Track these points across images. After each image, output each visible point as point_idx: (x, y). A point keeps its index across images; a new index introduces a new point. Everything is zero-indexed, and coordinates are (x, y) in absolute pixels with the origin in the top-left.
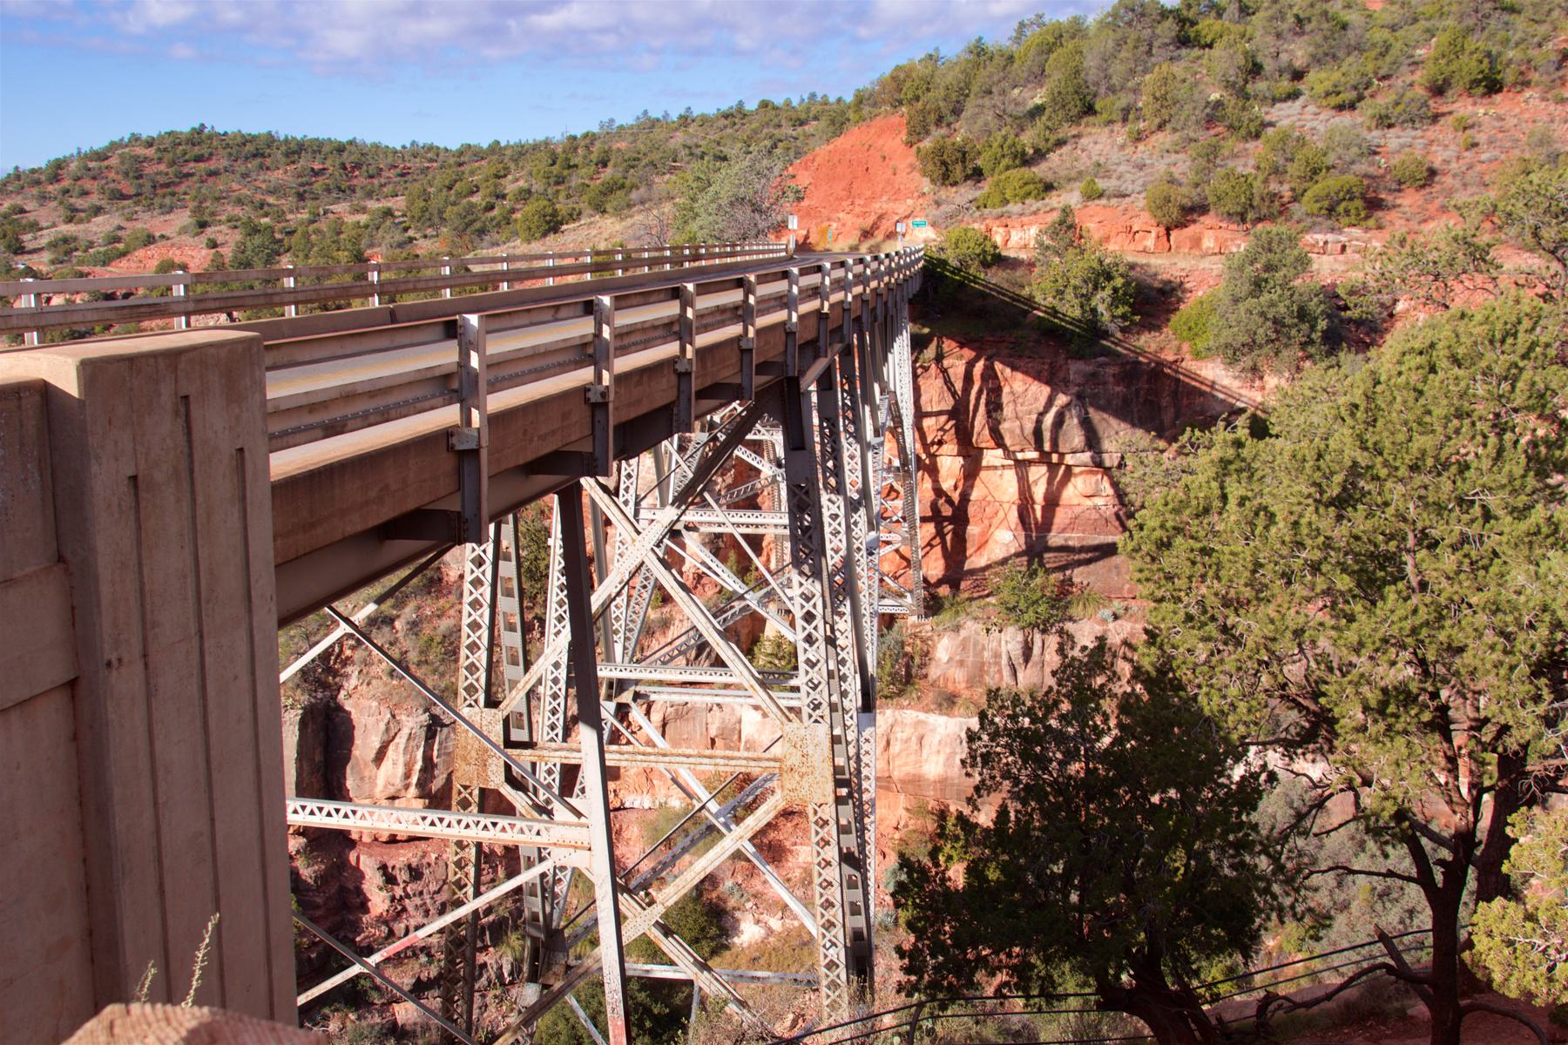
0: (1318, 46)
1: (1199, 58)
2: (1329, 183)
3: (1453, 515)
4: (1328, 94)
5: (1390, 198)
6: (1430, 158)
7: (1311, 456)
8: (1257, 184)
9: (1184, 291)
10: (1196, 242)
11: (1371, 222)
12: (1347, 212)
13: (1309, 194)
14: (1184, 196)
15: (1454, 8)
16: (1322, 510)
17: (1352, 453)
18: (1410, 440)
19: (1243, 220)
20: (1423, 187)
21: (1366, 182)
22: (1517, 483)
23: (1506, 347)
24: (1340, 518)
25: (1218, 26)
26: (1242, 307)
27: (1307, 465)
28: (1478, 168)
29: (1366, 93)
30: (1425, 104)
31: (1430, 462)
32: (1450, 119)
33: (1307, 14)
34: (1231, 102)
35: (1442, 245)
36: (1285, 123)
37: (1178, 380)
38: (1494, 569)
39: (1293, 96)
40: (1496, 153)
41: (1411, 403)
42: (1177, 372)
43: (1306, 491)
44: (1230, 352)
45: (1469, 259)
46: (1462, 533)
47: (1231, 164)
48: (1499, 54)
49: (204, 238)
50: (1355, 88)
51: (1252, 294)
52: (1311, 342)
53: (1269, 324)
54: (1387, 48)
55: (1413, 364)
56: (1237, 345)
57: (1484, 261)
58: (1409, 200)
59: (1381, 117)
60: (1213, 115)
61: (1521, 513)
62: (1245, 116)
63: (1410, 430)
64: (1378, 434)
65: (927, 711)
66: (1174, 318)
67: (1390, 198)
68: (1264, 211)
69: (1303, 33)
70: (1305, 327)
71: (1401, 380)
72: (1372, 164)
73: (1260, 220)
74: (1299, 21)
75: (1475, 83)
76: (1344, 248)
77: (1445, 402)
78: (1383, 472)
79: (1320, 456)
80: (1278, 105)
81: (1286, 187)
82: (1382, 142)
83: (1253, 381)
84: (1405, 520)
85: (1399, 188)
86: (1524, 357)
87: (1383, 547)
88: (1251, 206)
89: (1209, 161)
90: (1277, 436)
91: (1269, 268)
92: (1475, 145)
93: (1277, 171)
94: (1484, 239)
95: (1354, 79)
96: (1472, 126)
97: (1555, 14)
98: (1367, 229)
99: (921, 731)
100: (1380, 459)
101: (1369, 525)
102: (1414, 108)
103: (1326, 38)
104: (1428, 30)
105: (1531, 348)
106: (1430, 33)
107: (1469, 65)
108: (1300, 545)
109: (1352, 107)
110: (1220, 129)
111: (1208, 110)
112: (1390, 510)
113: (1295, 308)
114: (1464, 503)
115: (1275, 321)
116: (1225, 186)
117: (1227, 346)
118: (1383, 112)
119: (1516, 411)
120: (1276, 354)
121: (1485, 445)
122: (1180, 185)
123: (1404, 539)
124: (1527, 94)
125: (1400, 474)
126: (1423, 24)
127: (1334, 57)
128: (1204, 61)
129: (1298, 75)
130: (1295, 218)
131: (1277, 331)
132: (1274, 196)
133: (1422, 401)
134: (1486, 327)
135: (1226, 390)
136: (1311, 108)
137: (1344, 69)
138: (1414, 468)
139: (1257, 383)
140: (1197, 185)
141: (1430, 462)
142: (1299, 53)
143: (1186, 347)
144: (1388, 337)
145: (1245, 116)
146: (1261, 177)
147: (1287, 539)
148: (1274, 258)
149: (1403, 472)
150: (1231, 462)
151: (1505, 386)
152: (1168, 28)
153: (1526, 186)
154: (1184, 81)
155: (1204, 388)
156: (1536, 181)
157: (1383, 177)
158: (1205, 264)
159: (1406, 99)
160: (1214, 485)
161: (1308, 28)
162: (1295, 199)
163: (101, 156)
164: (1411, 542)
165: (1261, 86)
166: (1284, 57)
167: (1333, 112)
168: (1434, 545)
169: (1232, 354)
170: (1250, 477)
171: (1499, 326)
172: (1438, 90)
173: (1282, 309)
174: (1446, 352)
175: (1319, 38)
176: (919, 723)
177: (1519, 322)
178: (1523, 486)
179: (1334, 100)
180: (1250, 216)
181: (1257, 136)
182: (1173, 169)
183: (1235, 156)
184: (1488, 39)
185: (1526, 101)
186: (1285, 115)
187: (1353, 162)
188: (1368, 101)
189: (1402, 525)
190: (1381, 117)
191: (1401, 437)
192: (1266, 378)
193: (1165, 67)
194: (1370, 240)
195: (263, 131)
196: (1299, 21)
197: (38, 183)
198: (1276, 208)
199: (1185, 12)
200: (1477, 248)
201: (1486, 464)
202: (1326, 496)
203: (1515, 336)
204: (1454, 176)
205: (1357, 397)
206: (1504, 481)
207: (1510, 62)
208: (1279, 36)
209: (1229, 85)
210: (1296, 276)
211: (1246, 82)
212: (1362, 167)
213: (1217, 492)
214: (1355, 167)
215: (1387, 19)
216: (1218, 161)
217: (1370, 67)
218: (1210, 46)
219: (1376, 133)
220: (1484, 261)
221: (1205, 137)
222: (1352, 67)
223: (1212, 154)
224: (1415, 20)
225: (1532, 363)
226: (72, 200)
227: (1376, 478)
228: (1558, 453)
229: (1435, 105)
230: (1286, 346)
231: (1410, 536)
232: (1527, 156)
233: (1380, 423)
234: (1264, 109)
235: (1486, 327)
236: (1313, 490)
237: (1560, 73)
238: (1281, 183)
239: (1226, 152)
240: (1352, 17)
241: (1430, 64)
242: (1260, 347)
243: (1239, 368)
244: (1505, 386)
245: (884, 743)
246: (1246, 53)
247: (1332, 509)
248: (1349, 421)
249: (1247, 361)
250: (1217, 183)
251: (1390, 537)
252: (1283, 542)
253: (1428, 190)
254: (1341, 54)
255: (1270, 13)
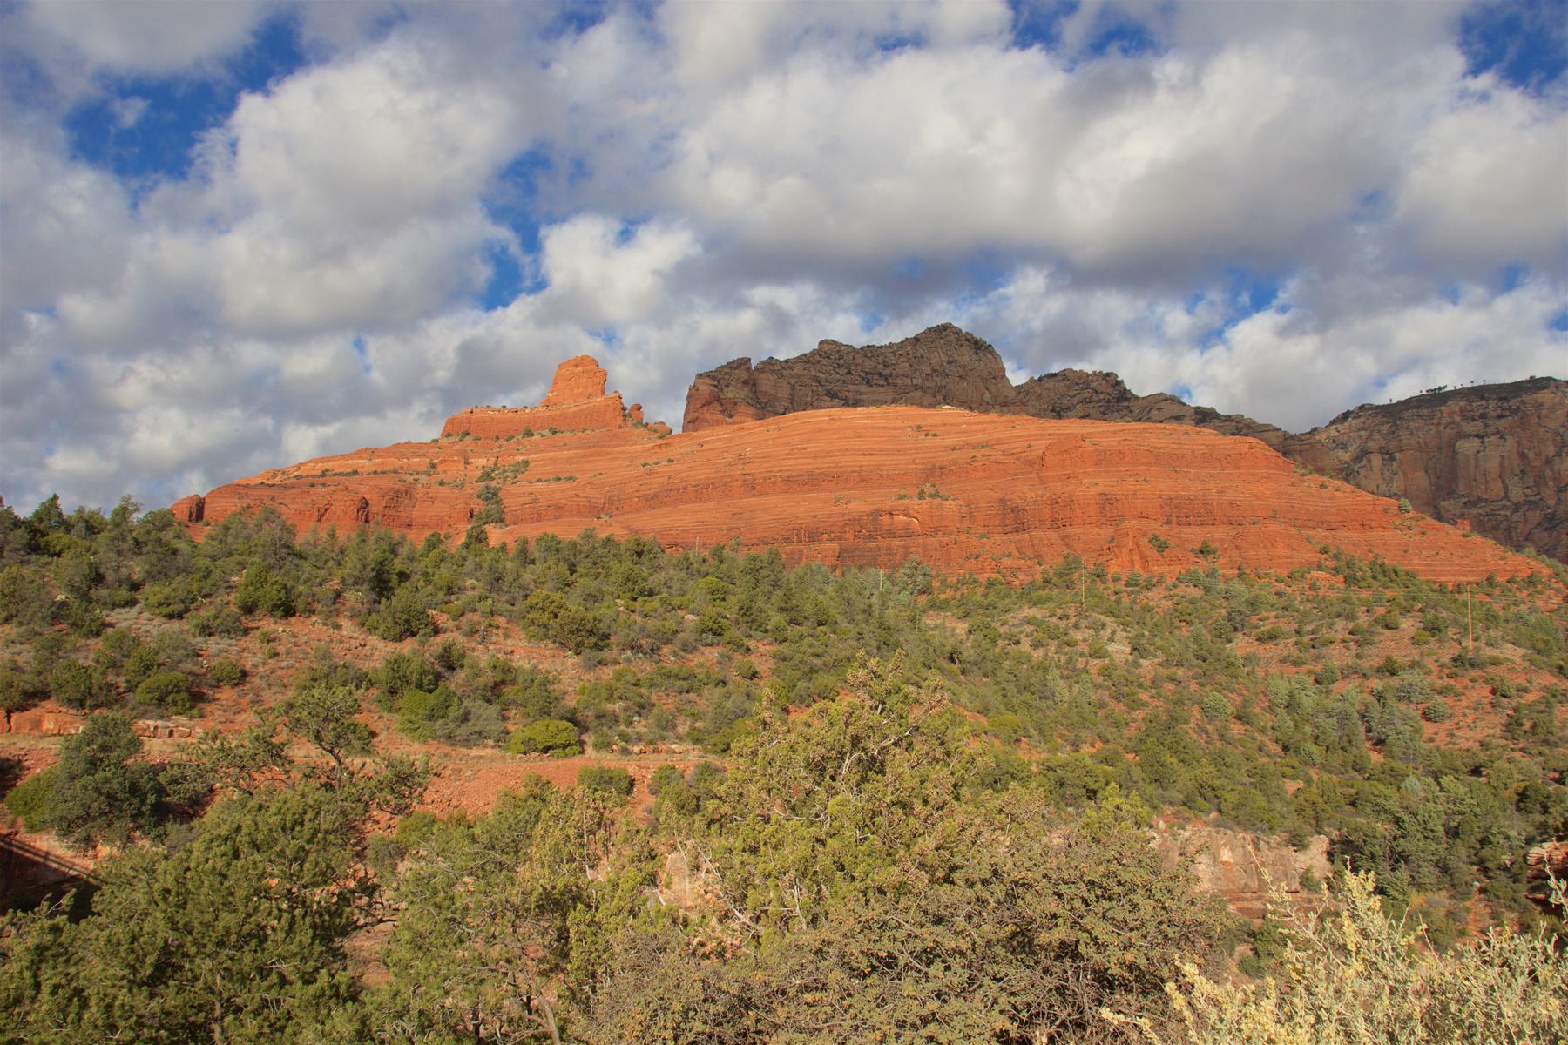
0: (152, 565)
1: (47, 564)
2: (160, 678)
3: (255, 983)
4: (160, 605)
5: (210, 692)
6: (242, 662)
7: (125, 938)
8: (95, 675)
9: (22, 769)
10: (37, 724)
11: (195, 712)
12: (175, 703)
13: (142, 686)
14: (26, 682)
15: (260, 549)
16: (135, 990)
17: (165, 933)
18: (216, 919)
19: (82, 706)
20: (237, 685)
21: (190, 679)
22: (306, 951)
23: (295, 833)
24: (152, 996)
25: (66, 539)
26: (78, 784)
27: (122, 949)
28: (280, 672)
29: (192, 606)
30: (238, 620)
31: (233, 938)
32: (258, 633)
33: (144, 539)
34: (76, 603)
35: (247, 743)
36: (123, 624)
37: (12, 852)
38: (289, 1030)
39: (131, 603)
40: (292, 662)
41: (217, 885)
42: (10, 844)
43: (120, 973)
44: (65, 825)
45: (268, 755)
46: (261, 999)
47: (73, 657)
48: (293, 587)
50: (183, 601)
51: (87, 772)
52: (142, 814)
53: (102, 798)
54: (209, 573)
55: (219, 851)
56: (72, 817)
57: (280, 757)
58: (226, 695)
59: (203, 627)
60: (59, 613)
61: (308, 980)
62: (88, 617)
63: (216, 910)
64: (193, 915)
66: (11, 794)
67: (210, 692)
68: (102, 699)
69: (141, 554)
70: (136, 801)
71: (209, 866)
72: (196, 664)
73: (97, 706)
74: (137, 543)
75: (275, 607)
76: (171, 733)
77: (245, 884)
78: (193, 950)
79: (134, 939)
80: (117, 610)
81: (122, 679)
82: (205, 647)
83: (86, 850)
84: (213, 992)
85: (218, 684)
86: (309, 841)
87: (192, 1019)
88: (90, 694)
89: (52, 653)
90: (100, 915)
91: (105, 748)
92: (276, 654)
93: (115, 665)
94: (283, 736)
95: (182, 594)
96: (274, 640)
97: (330, 563)
98: (192, 718)
100: (190, 938)
101: (179, 999)
102: (229, 622)
103: (159, 560)
104: (240, 563)
105: (314, 835)
106: (242, 565)
107: (271, 593)
108: (113, 1028)
109: (180, 616)
110: (64, 626)
111: (53, 609)
112: (200, 984)
113: (127, 784)
114: (263, 973)
115: (109, 796)
116: (67, 676)
117: (62, 818)
118: (205, 623)
119: (305, 887)
120: (109, 826)
121: (279, 920)
122: (24, 672)
123: (213, 1009)
124: (314, 619)
125: (207, 950)
126: (236, 558)
127: (166, 575)
128: (52, 567)
129: (135, 587)
130: (130, 705)
131: (110, 805)
132: (111, 686)
133: (227, 884)
134: (279, 817)
135: (61, 861)
136: (146, 615)
137: (174, 586)
138: (221, 944)
139: (91, 852)
140: (40, 673)
141: (233, 938)
142: (137, 569)
143: (21, 820)
144: (209, 809)
145: (88, 617)
146: (100, 670)
147: (100, 1023)
148: (109, 740)
149: (210, 948)
150: (47, 948)
151: (295, 866)
152: (20, 536)
153: (310, 699)
154: (33, 582)
155: (37, 858)
156: (317, 695)
157: (205, 674)
158: (44, 744)
159: (223, 615)
160: (27, 974)
161: (145, 550)
162: (130, 690)
164: (218, 1012)
165: (103, 592)
166: (124, 571)
167: (164, 620)
168: (239, 1010)
169: (66, 827)
170: (67, 961)
171: (289, 816)
172: (249, 609)
173: (116, 786)
174: (247, 839)
175: (154, 559)
177: (305, 813)
178: (311, 953)
179: (165, 610)
180: (88, 702)
181: (98, 634)
182: (17, 658)
183: (78, 650)
184: (284, 575)
185: (313, 625)
186: (123, 618)
187: (180, 662)
188: (194, 613)
189: (210, 997)
190: (203, 627)
191: (208, 917)
192: (99, 847)
193: (14, 569)
194: (194, 726)
196: (137, 543)
198: (113, 697)
199: (37, 525)
200: (274, 746)
201: (281, 936)
202: (138, 977)
203: (302, 824)
204: (261, 677)
205: (170, 882)
206: (296, 950)
207: (300, 594)
208: (119, 553)
209: (73, 589)
210: (129, 756)
211: (90, 588)
212: (188, 666)
213: (30, 982)
214: (182, 666)
215: (208, 550)
216: (61, 654)
217: (195, 586)
218: (59, 555)
219: (199, 639)
220: (280, 757)
221: (50, 632)
222: (179, 586)
223: (55, 647)
224: (230, 555)
225: (315, 847)
227: (186, 955)
228: (338, 920)
229: (246, 621)
230: (119, 818)
231: (218, 1006)
232: (315, 666)
233: (189, 906)
234: (105, 612)
235: (279, 817)
236: (126, 972)
237: (337, 606)
238: (118, 675)
239: (69, 646)
240: (182, 546)
241: (242, 588)
242: (94, 819)
243: (72, 839)
244: (295, 866)
246: (90, 564)
247: (144, 988)
248: (162, 906)
249: (81, 832)
250: (59, 672)
251: (200, 1008)
252: (96, 1027)
253: (241, 687)
254: (172, 574)
255: (113, 534)
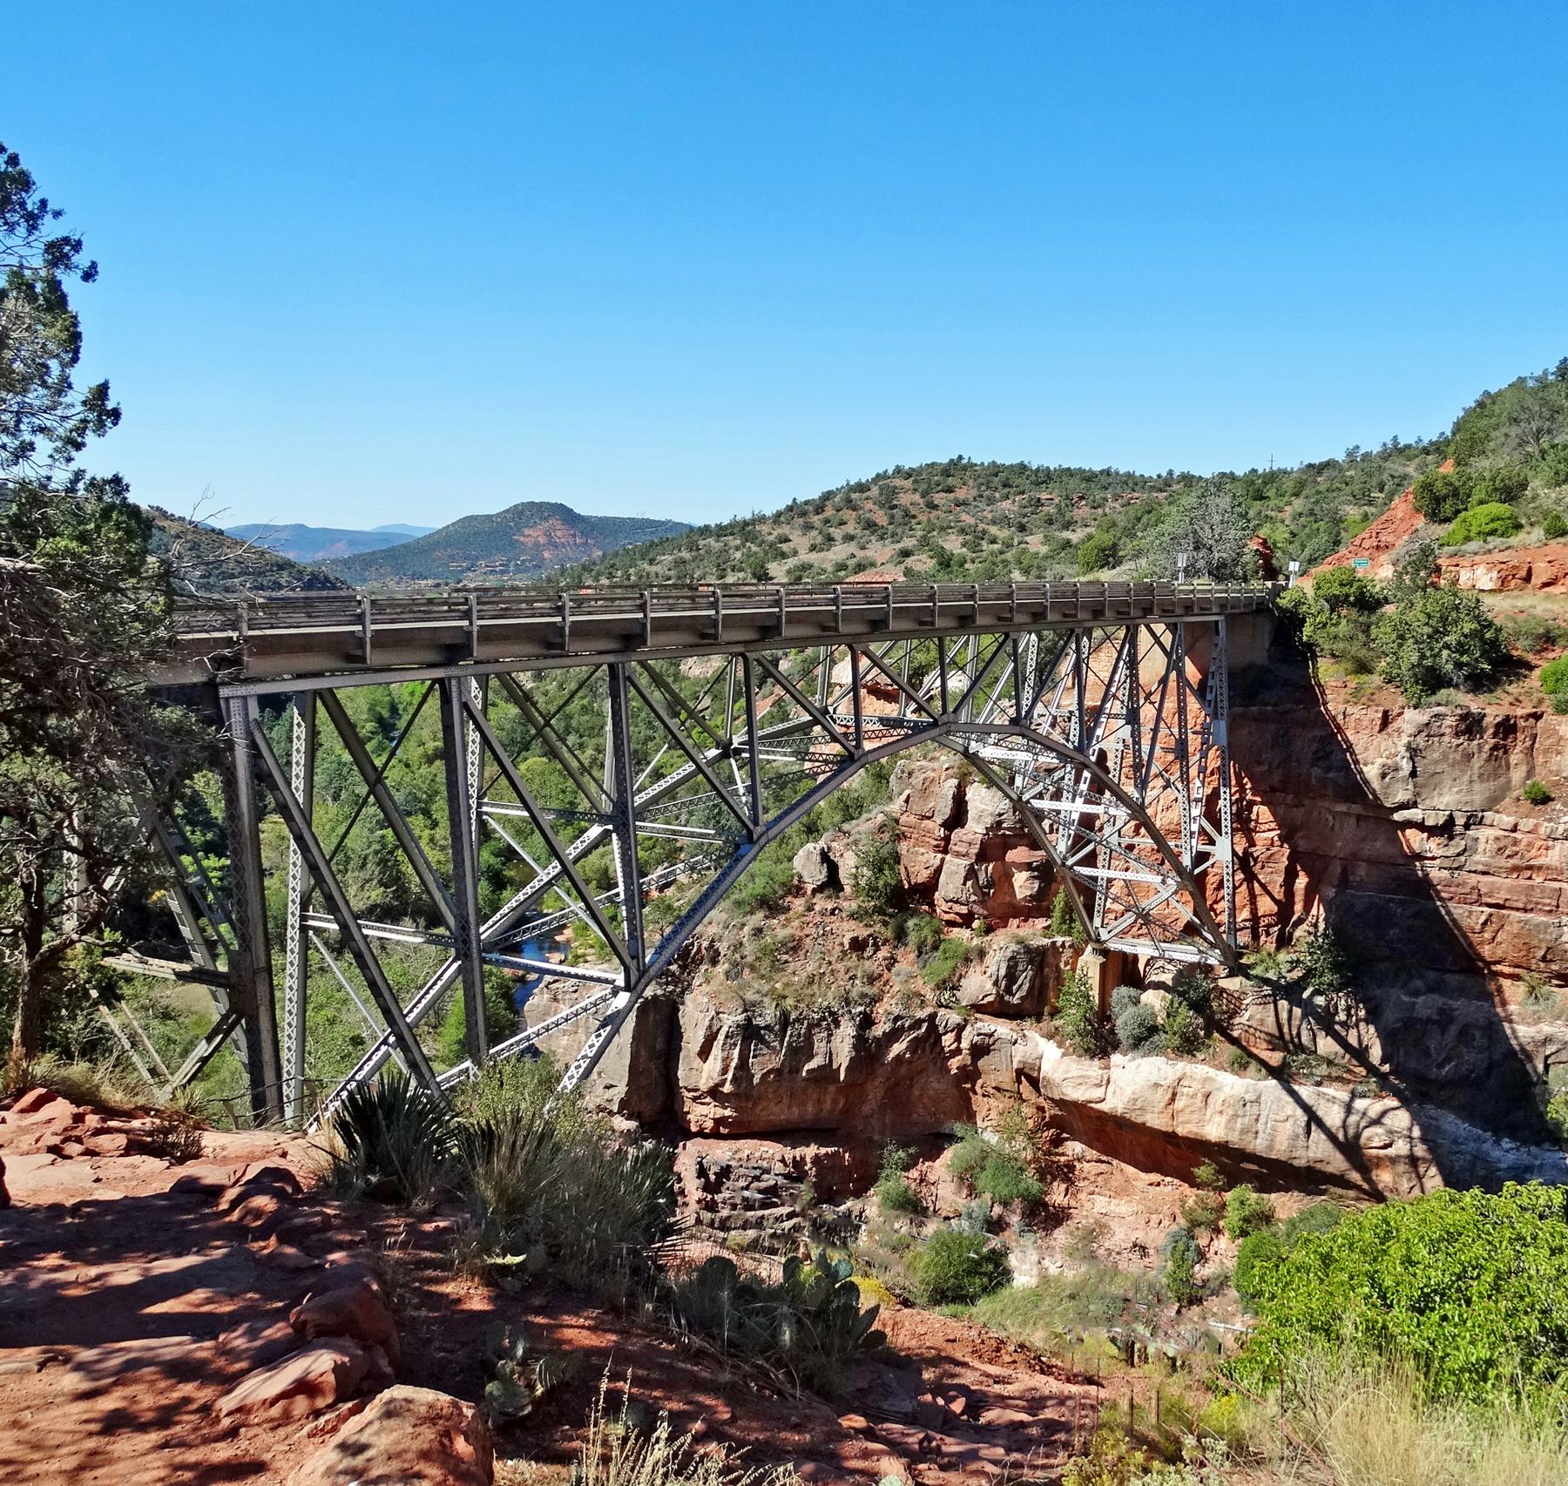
49: (902, 567)
65: (1220, 1068)
99: (1208, 1088)
163: (862, 488)
176: (1207, 1079)
195: (1016, 461)
197: (804, 514)
226: (832, 530)
245: (1169, 1095)
